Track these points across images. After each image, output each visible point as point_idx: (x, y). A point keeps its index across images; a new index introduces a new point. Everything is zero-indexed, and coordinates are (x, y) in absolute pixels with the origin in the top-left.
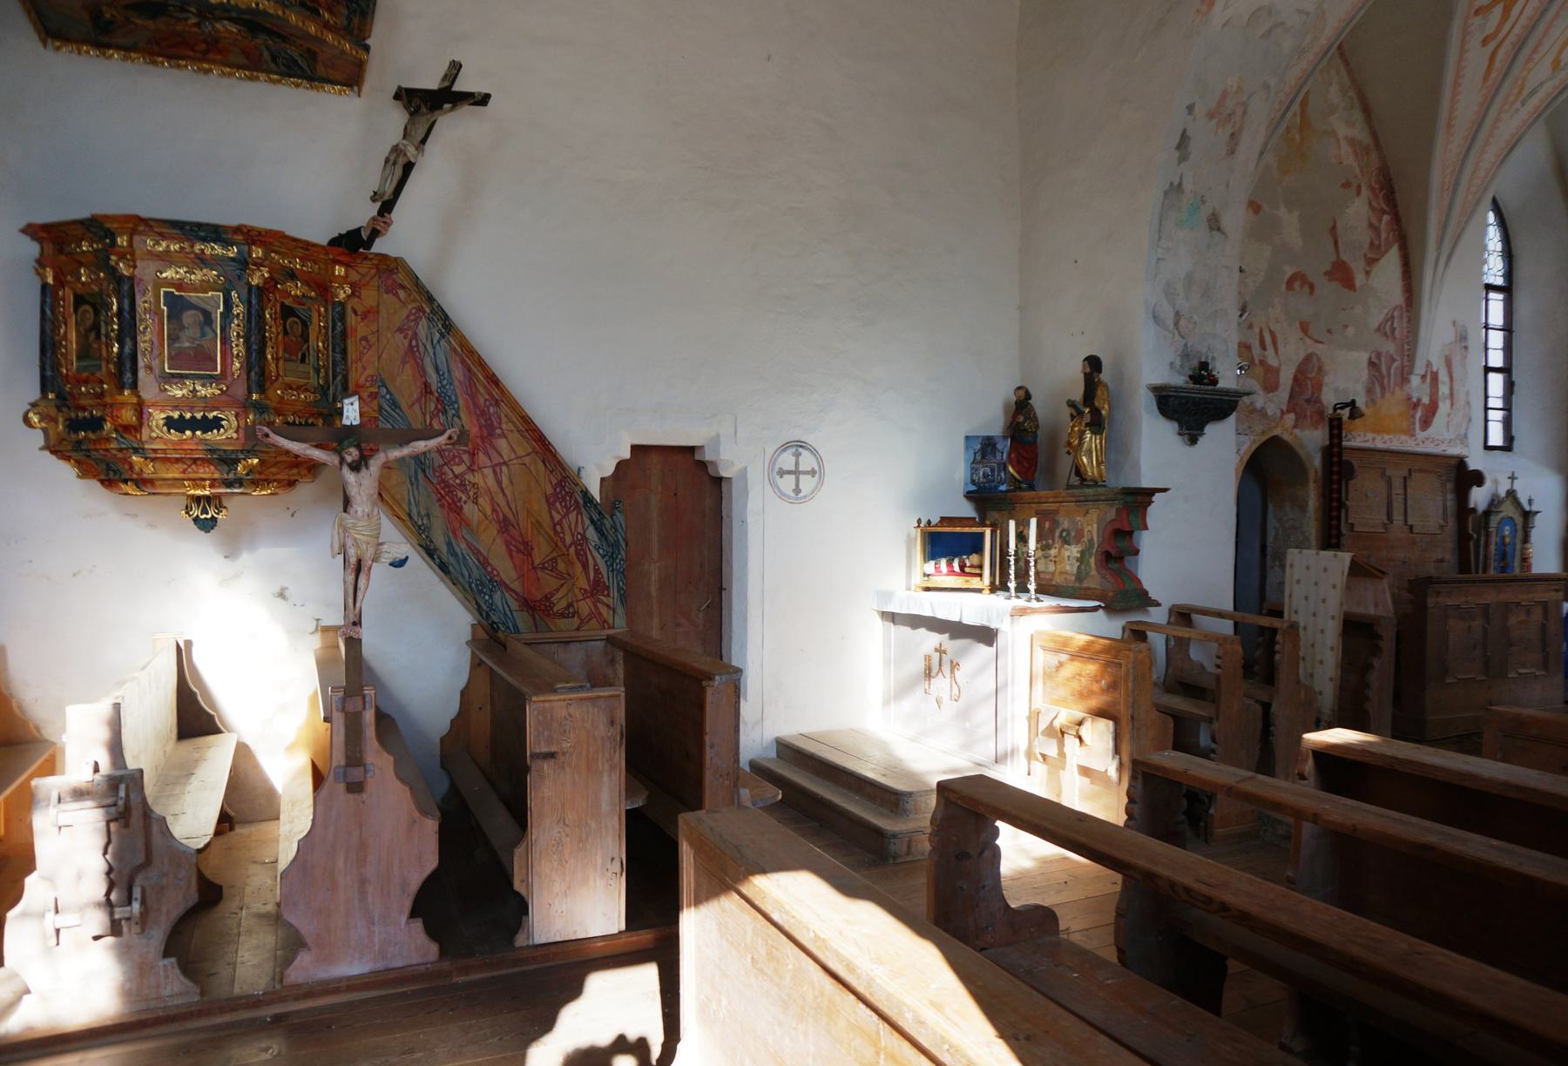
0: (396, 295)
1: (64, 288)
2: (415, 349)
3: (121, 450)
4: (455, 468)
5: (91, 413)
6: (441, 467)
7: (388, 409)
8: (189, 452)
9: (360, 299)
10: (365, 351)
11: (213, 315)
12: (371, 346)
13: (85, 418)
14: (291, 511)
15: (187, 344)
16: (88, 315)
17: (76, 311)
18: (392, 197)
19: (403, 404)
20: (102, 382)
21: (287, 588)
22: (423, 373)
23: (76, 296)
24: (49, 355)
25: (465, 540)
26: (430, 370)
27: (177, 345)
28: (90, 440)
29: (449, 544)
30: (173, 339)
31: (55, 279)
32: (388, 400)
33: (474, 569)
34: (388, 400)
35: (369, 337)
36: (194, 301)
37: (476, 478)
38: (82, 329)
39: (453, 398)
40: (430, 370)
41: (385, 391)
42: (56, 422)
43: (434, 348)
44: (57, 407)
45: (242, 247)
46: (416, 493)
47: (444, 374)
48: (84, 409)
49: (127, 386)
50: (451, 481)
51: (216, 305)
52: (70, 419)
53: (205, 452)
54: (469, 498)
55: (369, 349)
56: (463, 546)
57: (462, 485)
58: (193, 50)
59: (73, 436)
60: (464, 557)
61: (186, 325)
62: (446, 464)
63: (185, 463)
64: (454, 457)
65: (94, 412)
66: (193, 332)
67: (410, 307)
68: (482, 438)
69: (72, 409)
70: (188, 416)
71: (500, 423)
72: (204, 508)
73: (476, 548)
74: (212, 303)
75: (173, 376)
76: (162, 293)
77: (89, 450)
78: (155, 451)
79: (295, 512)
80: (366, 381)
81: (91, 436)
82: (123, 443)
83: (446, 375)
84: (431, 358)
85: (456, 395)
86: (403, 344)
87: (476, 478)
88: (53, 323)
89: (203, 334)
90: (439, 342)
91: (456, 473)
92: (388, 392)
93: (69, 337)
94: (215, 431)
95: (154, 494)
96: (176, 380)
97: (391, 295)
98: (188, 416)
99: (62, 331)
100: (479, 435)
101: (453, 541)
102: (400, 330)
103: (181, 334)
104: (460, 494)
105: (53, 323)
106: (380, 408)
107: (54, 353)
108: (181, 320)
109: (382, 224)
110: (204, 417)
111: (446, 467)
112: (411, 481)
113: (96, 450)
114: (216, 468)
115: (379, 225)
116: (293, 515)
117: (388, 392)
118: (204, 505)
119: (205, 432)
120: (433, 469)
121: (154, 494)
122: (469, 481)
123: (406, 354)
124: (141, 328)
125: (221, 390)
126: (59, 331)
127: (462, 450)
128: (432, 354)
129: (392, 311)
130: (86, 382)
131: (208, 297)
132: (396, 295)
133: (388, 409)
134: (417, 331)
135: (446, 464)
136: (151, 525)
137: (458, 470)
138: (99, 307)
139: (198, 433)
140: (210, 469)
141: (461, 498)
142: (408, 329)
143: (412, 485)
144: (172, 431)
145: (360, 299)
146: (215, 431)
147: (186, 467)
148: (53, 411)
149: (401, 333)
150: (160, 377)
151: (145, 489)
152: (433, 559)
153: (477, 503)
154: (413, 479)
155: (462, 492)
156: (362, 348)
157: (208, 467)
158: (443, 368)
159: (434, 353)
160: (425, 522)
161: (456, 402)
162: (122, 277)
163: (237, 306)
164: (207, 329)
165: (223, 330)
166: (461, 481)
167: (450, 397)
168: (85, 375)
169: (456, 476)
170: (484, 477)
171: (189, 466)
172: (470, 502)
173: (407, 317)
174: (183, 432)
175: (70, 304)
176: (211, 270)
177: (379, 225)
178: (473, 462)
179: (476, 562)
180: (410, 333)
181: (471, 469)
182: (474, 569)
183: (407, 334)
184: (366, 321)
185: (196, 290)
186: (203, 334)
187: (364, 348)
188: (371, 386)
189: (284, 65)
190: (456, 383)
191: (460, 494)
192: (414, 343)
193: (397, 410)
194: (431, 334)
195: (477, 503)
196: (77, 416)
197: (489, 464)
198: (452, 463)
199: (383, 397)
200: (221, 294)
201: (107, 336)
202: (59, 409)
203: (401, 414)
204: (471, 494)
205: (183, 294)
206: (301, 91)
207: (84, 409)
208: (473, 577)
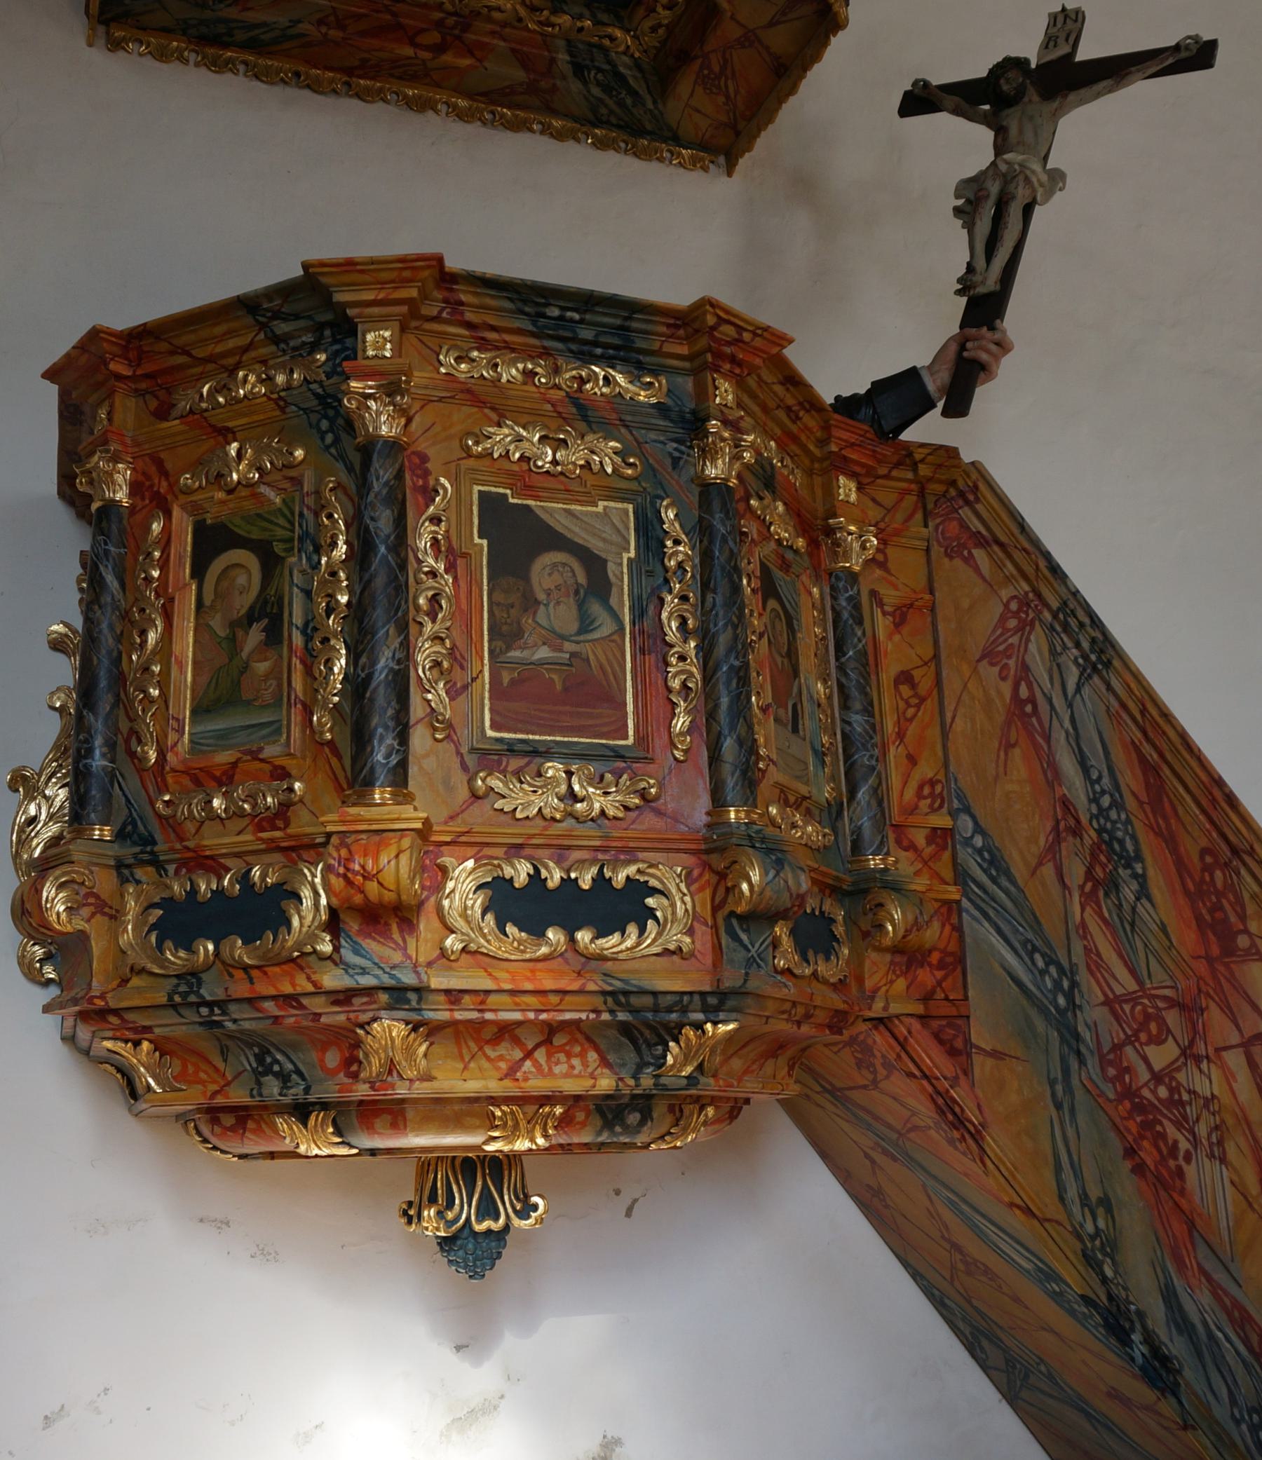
0: (969, 560)
1: (168, 514)
2: (1029, 709)
3: (343, 997)
4: (1150, 1051)
5: (245, 878)
6: (1117, 1048)
7: (983, 878)
8: (554, 999)
9: (887, 570)
10: (911, 711)
11: (611, 567)
12: (923, 700)
13: (219, 893)
14: (625, 1200)
15: (543, 653)
16: (242, 580)
17: (199, 572)
18: (998, 287)
19: (1019, 870)
20: (282, 774)
21: (617, 1442)
22: (1053, 775)
23: (200, 530)
24: (105, 705)
25: (1209, 1279)
26: (1068, 765)
27: (515, 654)
28: (230, 967)
29: (1169, 1296)
30: (505, 635)
31: (135, 488)
32: (979, 852)
33: (1240, 1371)
34: (979, 852)
35: (916, 673)
36: (562, 524)
37: (1204, 1081)
38: (217, 623)
39: (1129, 846)
40: (1068, 765)
41: (970, 824)
42: (116, 916)
43: (1070, 706)
44: (120, 866)
45: (680, 379)
46: (1070, 1132)
47: (1100, 777)
48: (213, 865)
49: (381, 776)
50: (1146, 1093)
51: (616, 538)
52: (168, 903)
53: (598, 1001)
54: (1195, 1141)
55: (918, 706)
56: (1205, 1298)
57: (1175, 1102)
58: (413, 44)
59: (175, 957)
60: (1211, 1336)
61: (542, 596)
62: (1129, 1041)
63: (517, 1041)
64: (1148, 1017)
65: (256, 872)
66: (563, 616)
67: (1005, 594)
68: (1209, 960)
69: (171, 868)
70: (555, 877)
71: (1243, 917)
72: (486, 1194)
73: (1236, 1304)
74: (608, 532)
75: (511, 749)
76: (475, 497)
77: (222, 1004)
78: (453, 996)
79: (635, 1201)
80: (919, 796)
81: (238, 949)
82: (364, 971)
83: (1106, 781)
84: (1067, 732)
85: (1134, 838)
86: (999, 692)
87: (1204, 1081)
88: (125, 616)
89: (586, 625)
90: (1078, 689)
91: (1157, 1067)
92: (978, 829)
93: (176, 649)
94: (632, 929)
95: (272, 1155)
96: (515, 763)
97: (958, 562)
98: (555, 877)
99: (152, 637)
100: (1203, 953)
101: (1178, 1283)
102: (988, 655)
103: (527, 622)
104: (1172, 1131)
105: (125, 616)
106: (961, 877)
107: (121, 701)
108: (526, 579)
109: (993, 347)
110: (601, 881)
111: (1129, 1050)
112: (1053, 1094)
113: (252, 1001)
114: (604, 1062)
115: (988, 351)
116: (629, 1213)
117: (978, 829)
118: (485, 1185)
119: (601, 934)
120: (1102, 1057)
121: (272, 1155)
122: (1191, 1092)
123: (1008, 723)
124: (422, 601)
125: (643, 794)
126: (143, 633)
127: (1165, 998)
128: (1067, 724)
129: (966, 603)
130: (225, 779)
131: (597, 514)
132: (969, 560)
133: (983, 878)
134: (1028, 659)
135: (1129, 1041)
136: (265, 1253)
137: (1162, 1056)
138: (278, 548)
139: (583, 936)
140: (585, 1065)
141: (1176, 1142)
142: (1007, 654)
143: (1058, 1106)
144: (510, 929)
145: (887, 570)
146: (632, 929)
147: (518, 1054)
148: (105, 882)
149: (992, 664)
150: (473, 750)
151: (354, 1141)
152: (1124, 1340)
153: (1223, 1160)
154: (1059, 1088)
155: (1178, 1125)
156: (902, 705)
157: (582, 1055)
158: (1097, 762)
159: (1073, 720)
160: (1101, 1224)
161: (1139, 857)
162: (369, 448)
163: (677, 542)
164: (596, 608)
165: (639, 612)
166: (1172, 1090)
167: (1121, 842)
168: (224, 757)
169: (1157, 1078)
170: (1229, 1077)
171: (528, 1055)
172: (1202, 1156)
173: (1003, 619)
174: (541, 934)
175: (181, 558)
176: (608, 438)
177: (988, 351)
178: (1195, 1032)
179: (1242, 1348)
180: (1012, 663)
181: (1188, 1054)
182: (1240, 1371)
183: (1006, 666)
184: (906, 630)
185: (569, 495)
186: (586, 625)
187: (909, 705)
188: (933, 810)
189: (598, 84)
190: (1131, 803)
191: (1172, 1131)
192: (1024, 692)
193: (1004, 882)
194: (1058, 665)
195: (1223, 1160)
196: (194, 891)
197: (1235, 1039)
198: (1143, 1037)
199: (968, 842)
200: (630, 507)
201: (310, 629)
202: (121, 868)
203: (1012, 889)
204: (1202, 1130)
205: (531, 502)
206: (611, 157)
207: (213, 865)
208: (1241, 1401)
